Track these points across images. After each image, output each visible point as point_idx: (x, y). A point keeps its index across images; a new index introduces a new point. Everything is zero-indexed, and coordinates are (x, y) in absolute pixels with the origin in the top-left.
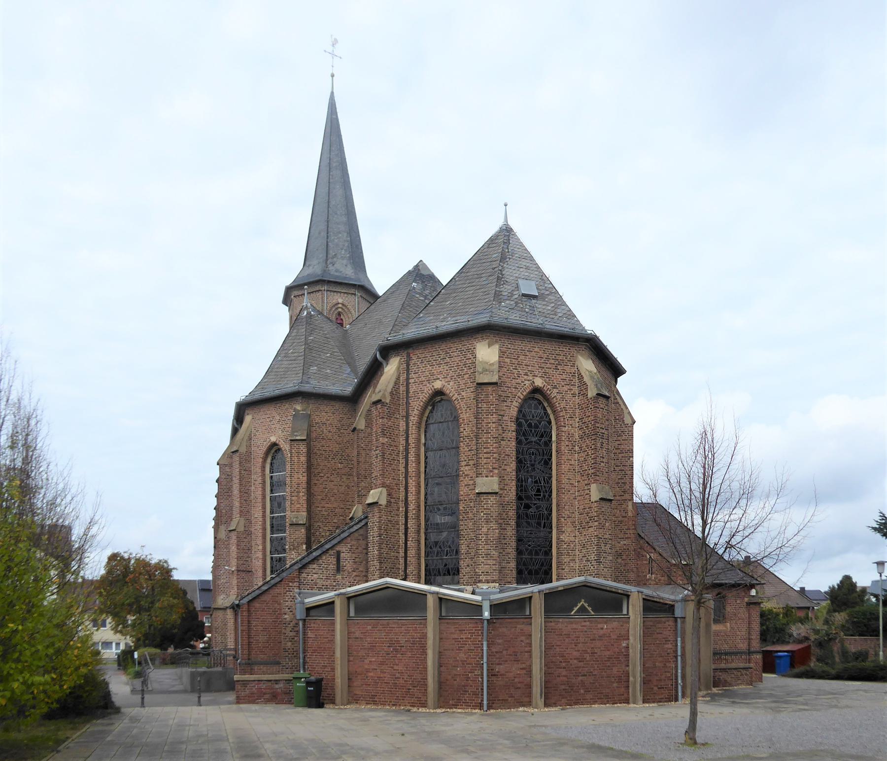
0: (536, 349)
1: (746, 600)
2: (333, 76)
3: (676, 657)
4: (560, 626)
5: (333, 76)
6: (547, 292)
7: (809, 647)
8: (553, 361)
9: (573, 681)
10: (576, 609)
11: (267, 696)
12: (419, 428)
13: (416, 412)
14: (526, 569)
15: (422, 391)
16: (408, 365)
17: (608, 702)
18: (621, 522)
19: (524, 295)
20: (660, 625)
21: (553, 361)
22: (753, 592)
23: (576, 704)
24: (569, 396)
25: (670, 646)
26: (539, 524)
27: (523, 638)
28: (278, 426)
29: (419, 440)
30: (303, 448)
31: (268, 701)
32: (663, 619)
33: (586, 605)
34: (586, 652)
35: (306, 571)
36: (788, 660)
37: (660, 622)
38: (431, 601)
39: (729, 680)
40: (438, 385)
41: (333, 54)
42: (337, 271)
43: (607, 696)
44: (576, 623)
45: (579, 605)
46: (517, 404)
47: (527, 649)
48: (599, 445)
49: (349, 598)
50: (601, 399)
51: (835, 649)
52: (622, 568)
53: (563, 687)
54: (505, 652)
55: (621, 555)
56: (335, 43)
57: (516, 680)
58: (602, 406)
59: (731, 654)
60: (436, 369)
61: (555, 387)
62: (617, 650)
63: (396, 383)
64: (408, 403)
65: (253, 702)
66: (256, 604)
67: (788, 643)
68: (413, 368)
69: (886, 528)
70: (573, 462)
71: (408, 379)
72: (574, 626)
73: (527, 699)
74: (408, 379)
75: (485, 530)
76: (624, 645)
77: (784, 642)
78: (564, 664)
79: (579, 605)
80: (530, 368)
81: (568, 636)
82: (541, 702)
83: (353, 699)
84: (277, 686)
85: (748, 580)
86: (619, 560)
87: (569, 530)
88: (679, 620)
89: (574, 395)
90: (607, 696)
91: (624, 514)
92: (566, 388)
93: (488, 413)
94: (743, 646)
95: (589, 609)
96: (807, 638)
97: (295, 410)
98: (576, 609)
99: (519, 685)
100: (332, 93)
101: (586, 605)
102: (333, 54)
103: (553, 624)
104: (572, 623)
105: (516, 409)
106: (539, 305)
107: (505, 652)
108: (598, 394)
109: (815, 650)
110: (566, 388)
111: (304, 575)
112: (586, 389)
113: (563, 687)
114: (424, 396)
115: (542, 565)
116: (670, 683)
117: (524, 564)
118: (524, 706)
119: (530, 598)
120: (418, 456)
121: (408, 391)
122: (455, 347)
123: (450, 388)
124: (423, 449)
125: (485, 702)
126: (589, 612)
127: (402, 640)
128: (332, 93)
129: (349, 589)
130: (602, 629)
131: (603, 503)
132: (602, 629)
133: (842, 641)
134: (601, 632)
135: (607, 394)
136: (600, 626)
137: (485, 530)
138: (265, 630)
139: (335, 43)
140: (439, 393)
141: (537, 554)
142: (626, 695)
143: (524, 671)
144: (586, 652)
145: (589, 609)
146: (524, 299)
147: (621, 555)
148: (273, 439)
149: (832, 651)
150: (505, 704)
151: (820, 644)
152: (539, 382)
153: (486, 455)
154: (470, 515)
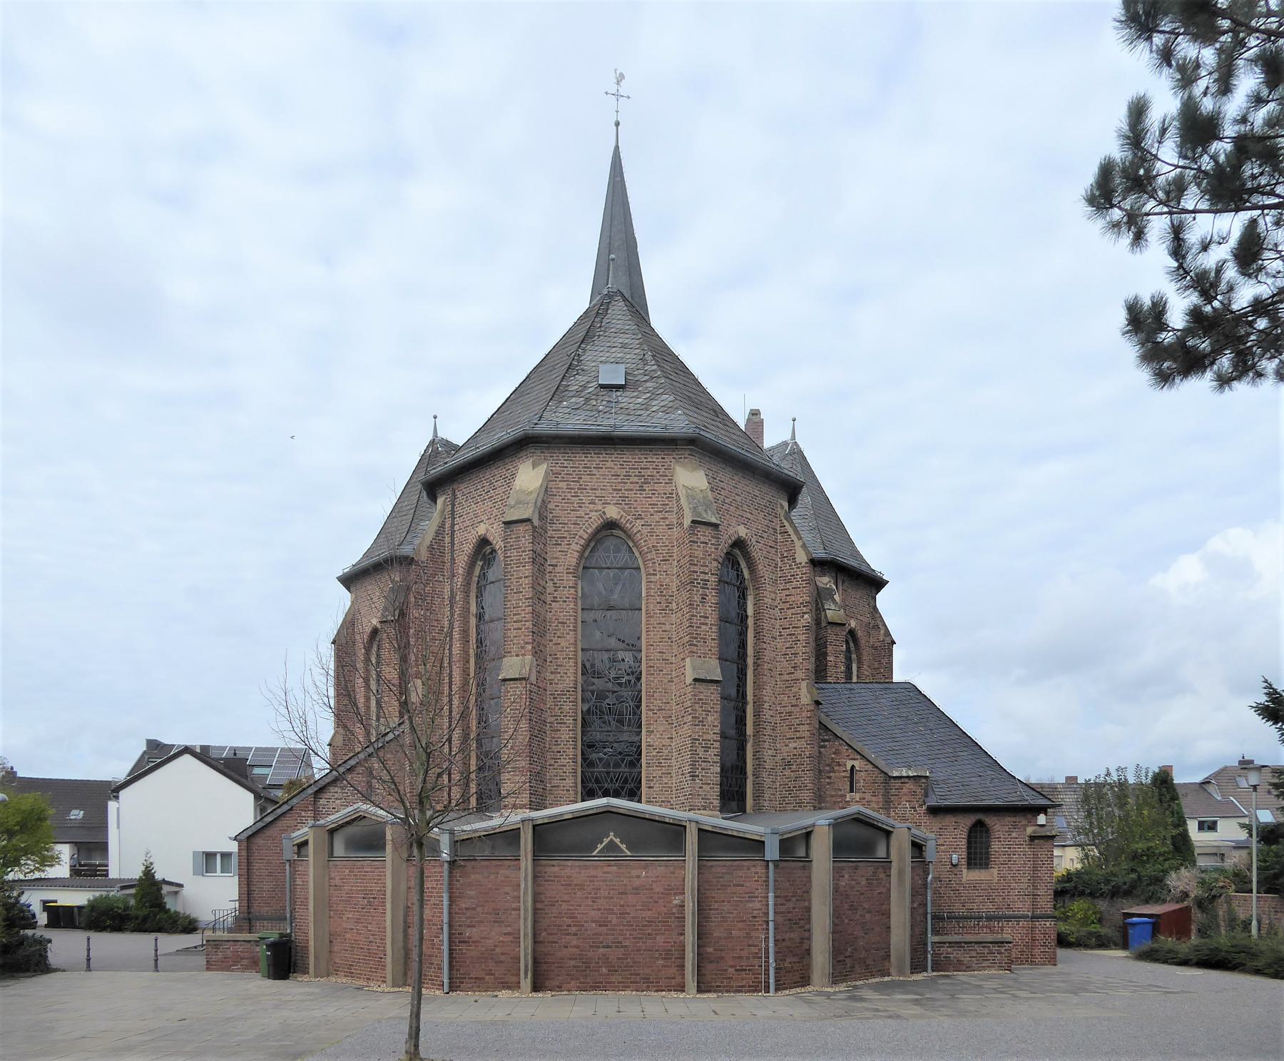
0: (609, 464)
1: (1030, 830)
2: (617, 124)
3: (767, 922)
4: (568, 871)
5: (617, 124)
7: (1188, 909)
8: (636, 479)
9: (590, 954)
10: (600, 847)
11: (245, 962)
12: (467, 594)
13: (461, 571)
14: (600, 788)
16: (453, 505)
17: (648, 989)
18: (790, 713)
19: (603, 386)
20: (740, 873)
21: (636, 479)
22: (1042, 819)
23: (595, 988)
24: (660, 530)
25: (758, 905)
26: (621, 722)
27: (508, 889)
29: (466, 610)
31: (245, 968)
32: (746, 863)
33: (617, 841)
34: (610, 911)
35: (328, 795)
36: (1149, 928)
37: (739, 868)
39: (966, 959)
41: (618, 96)
43: (646, 979)
44: (596, 868)
45: (606, 841)
46: (578, 548)
47: (514, 905)
48: (697, 598)
49: (332, 832)
50: (701, 528)
51: (1221, 913)
52: (791, 785)
53: (572, 963)
54: (479, 909)
55: (789, 763)
56: (620, 79)
57: (498, 950)
58: (702, 539)
59: (999, 918)
61: (639, 517)
62: (665, 910)
63: (437, 533)
64: (453, 559)
65: (228, 969)
66: (259, 841)
67: (1164, 901)
68: (458, 509)
69: (1283, 710)
70: (667, 627)
71: (453, 525)
72: (593, 873)
73: (514, 979)
74: (453, 525)
76: (676, 902)
77: (1150, 899)
78: (574, 929)
79: (606, 841)
80: (598, 493)
81: (581, 887)
82: (526, 983)
83: (329, 970)
84: (258, 949)
85: (1044, 802)
86: (787, 773)
87: (661, 729)
88: (771, 865)
89: (670, 527)
90: (646, 979)
91: (794, 702)
92: (657, 517)
93: (519, 564)
94: (1023, 907)
95: (623, 847)
96: (1185, 895)
98: (600, 847)
99: (502, 958)
100: (617, 147)
101: (617, 841)
102: (618, 96)
103: (556, 869)
104: (586, 867)
105: (576, 555)
106: (624, 398)
107: (479, 909)
108: (693, 522)
109: (1197, 915)
110: (657, 517)
111: (322, 802)
113: (572, 963)
115: (626, 781)
116: (756, 962)
117: (597, 781)
118: (509, 988)
119: (808, 835)
120: (465, 633)
121: (452, 543)
124: (473, 621)
125: (446, 981)
126: (622, 851)
128: (617, 147)
129: (332, 817)
130: (638, 877)
131: (701, 687)
132: (638, 877)
133: (1229, 901)
134: (637, 882)
135: (714, 520)
136: (634, 873)
138: (270, 874)
139: (620, 79)
141: (617, 765)
142: (678, 979)
143: (510, 938)
144: (610, 911)
145: (623, 847)
146: (603, 392)
147: (789, 763)
149: (1216, 916)
150: (480, 984)
151: (1200, 903)
152: (613, 513)
153: (516, 625)
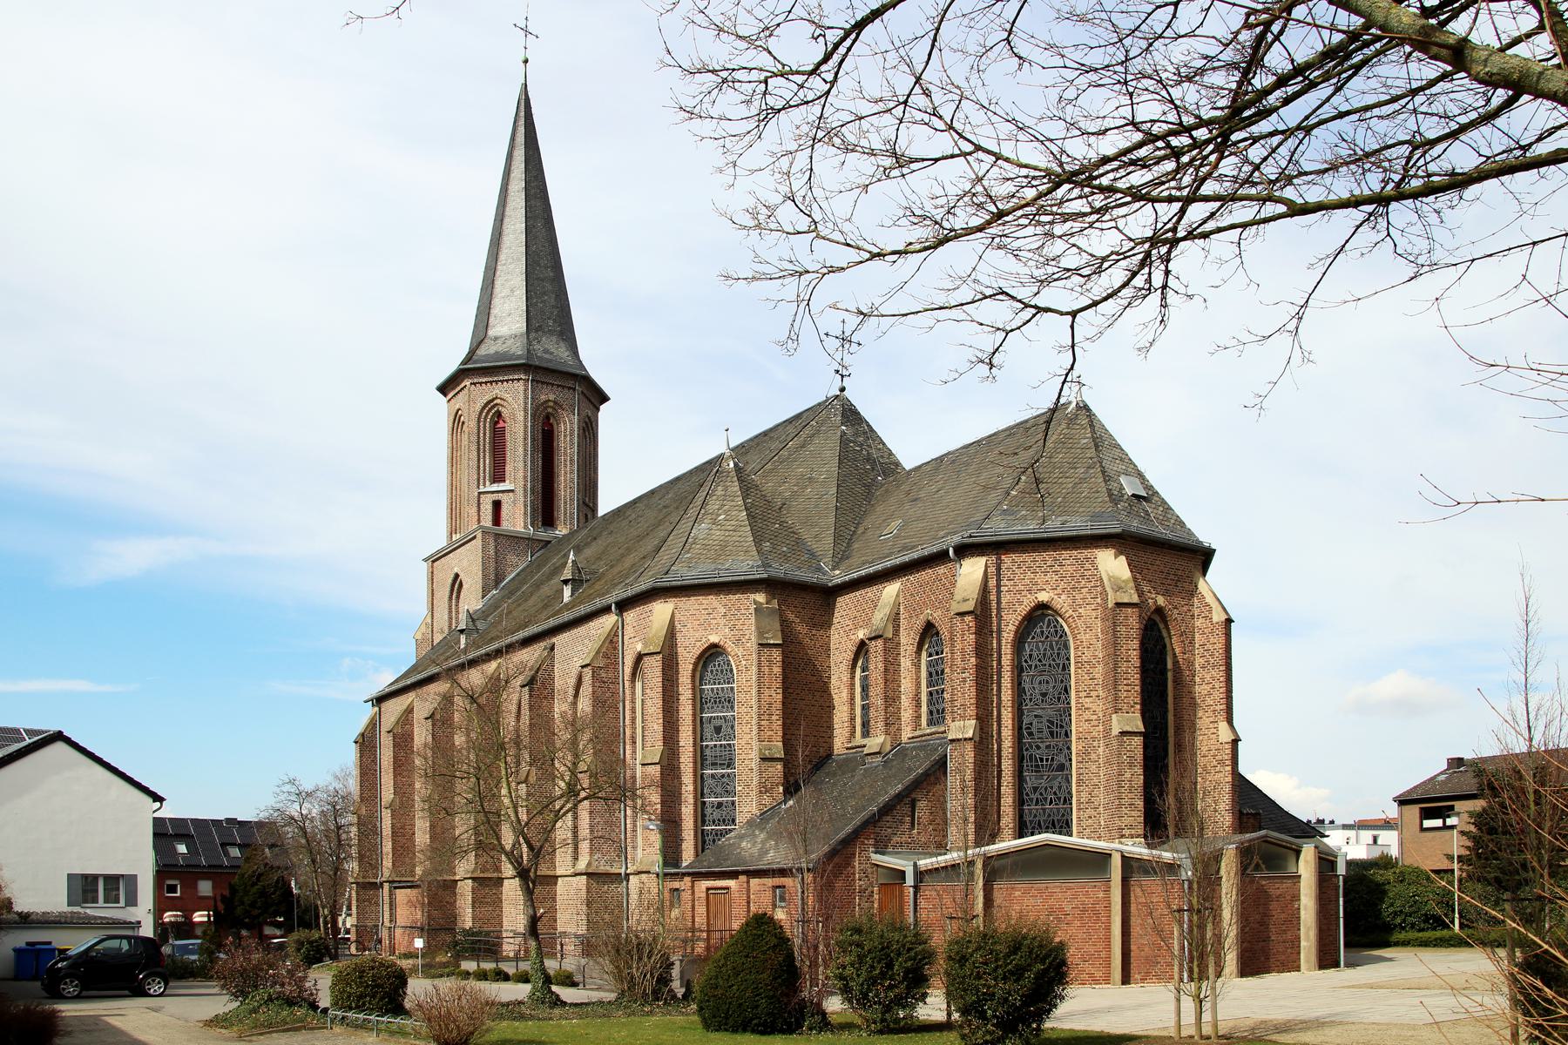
5: (526, 61)
6: (1148, 497)
15: (1021, 603)
28: (723, 621)
30: (777, 655)
38: (1116, 861)
40: (1043, 597)
42: (546, 351)
60: (1040, 578)
75: (1128, 775)
97: (755, 602)
112: (1210, 612)
114: (1023, 609)
122: (1068, 556)
123: (1061, 602)
127: (1068, 908)
137: (1128, 775)
140: (1043, 607)
148: (714, 639)
154: (1093, 756)
